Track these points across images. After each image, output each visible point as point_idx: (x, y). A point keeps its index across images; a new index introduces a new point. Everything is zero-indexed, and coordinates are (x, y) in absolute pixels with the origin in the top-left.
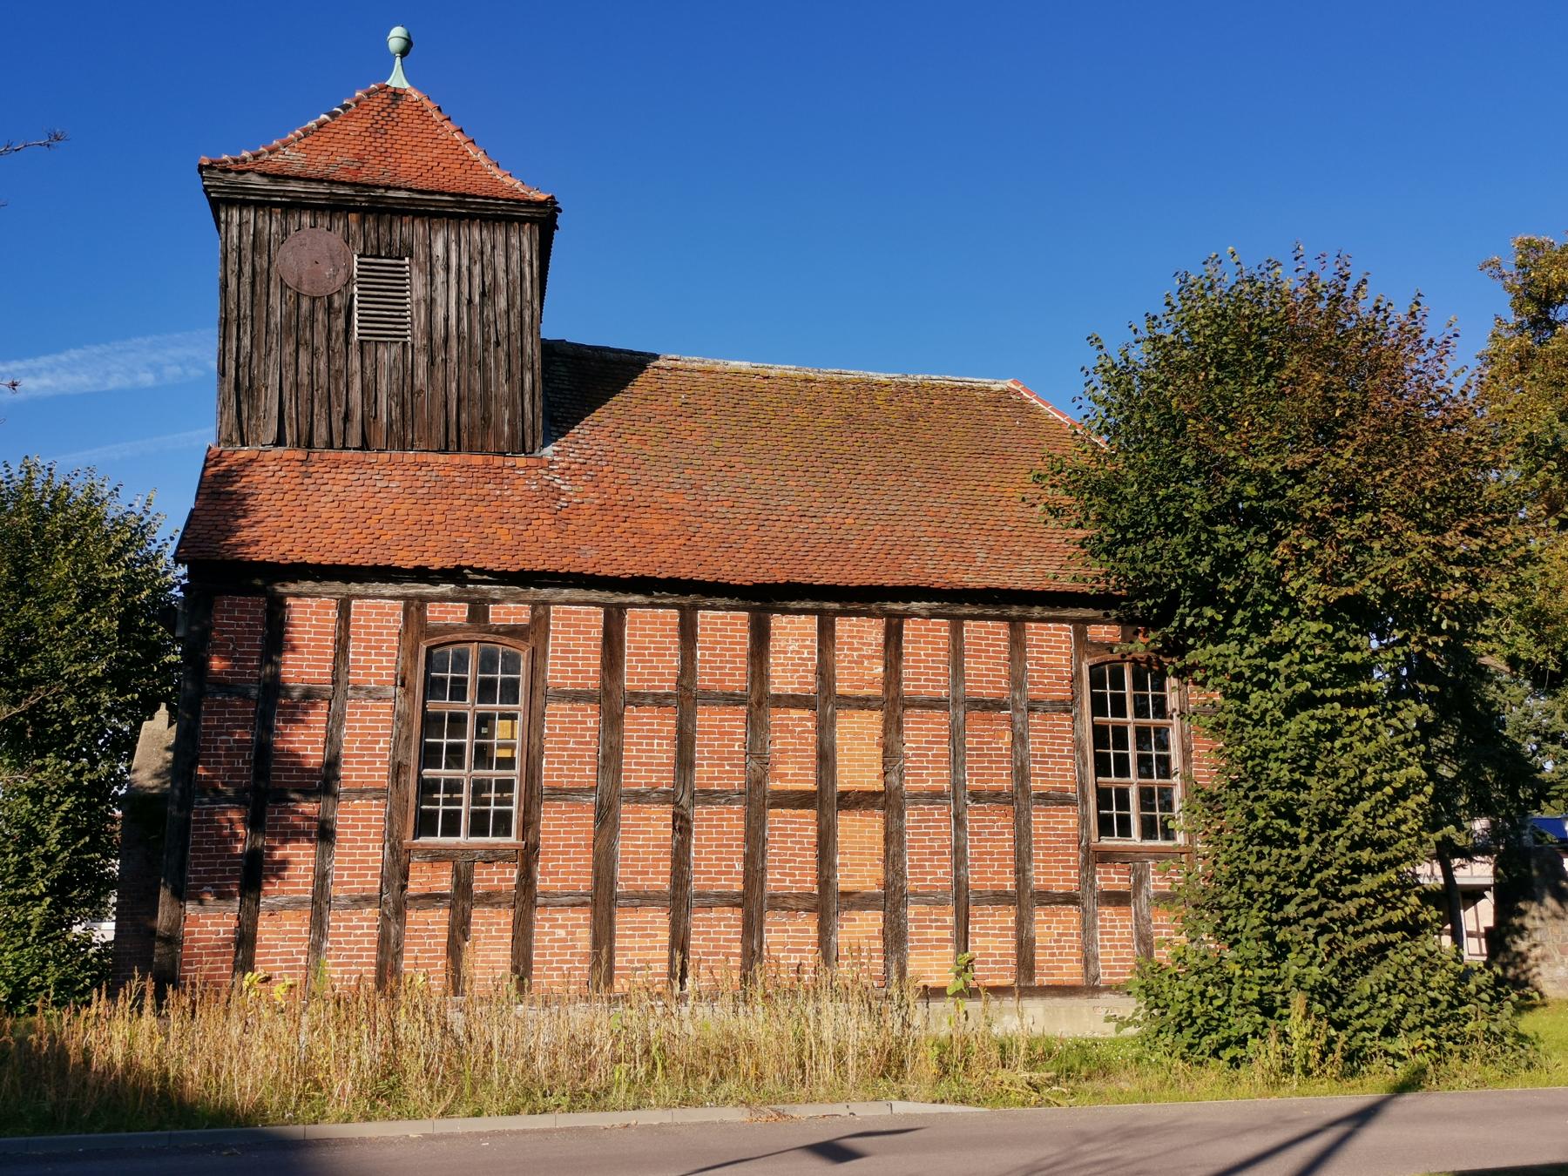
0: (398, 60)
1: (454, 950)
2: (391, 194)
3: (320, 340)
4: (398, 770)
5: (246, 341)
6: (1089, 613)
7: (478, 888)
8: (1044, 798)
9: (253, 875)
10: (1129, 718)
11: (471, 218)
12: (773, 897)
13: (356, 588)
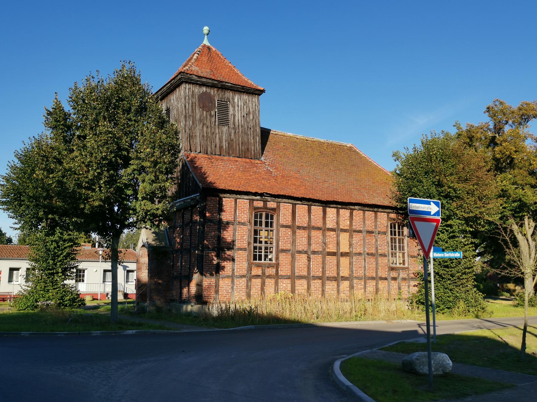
0: (206, 36)
1: (262, 289)
2: (227, 84)
3: (208, 124)
4: (249, 243)
5: (191, 123)
6: (390, 211)
7: (267, 274)
8: (381, 255)
9: (218, 269)
10: (397, 236)
11: (244, 92)
12: (328, 277)
13: (239, 196)
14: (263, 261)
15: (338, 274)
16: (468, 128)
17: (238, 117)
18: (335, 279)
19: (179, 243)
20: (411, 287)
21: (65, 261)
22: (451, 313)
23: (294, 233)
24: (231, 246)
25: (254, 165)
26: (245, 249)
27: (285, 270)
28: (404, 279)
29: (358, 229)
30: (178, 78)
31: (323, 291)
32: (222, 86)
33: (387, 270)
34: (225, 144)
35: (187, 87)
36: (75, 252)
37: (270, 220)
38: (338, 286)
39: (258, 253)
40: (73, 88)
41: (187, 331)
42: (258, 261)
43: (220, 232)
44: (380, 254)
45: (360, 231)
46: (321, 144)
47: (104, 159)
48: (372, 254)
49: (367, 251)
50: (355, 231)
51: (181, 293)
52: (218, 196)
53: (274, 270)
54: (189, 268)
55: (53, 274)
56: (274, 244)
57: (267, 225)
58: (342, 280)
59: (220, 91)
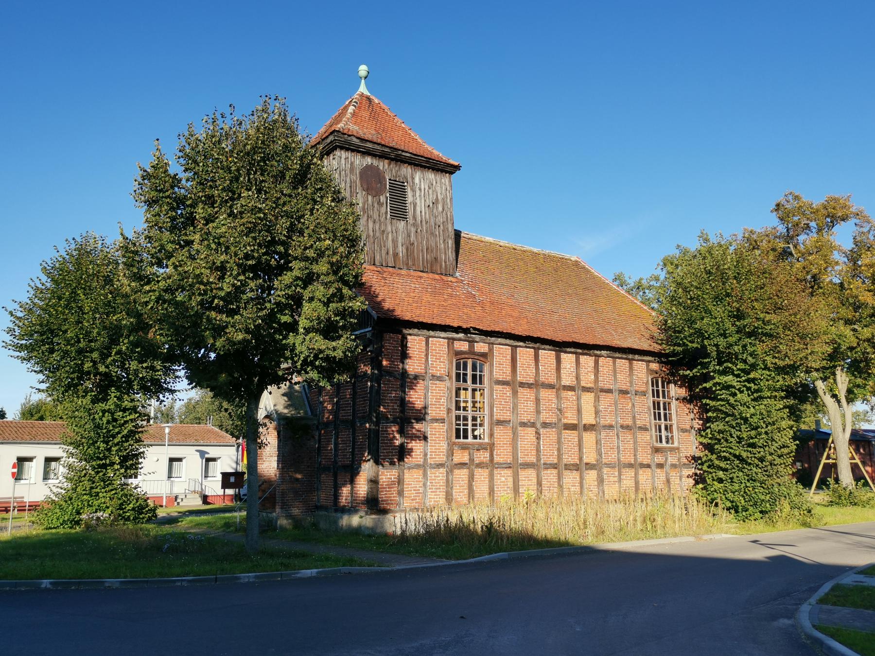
0: (363, 81)
2: (404, 154)
3: (376, 216)
4: (449, 411)
7: (477, 461)
9: (402, 453)
11: (429, 168)
12: (566, 465)
13: (432, 333)
14: (470, 439)
15: (581, 459)
16: (746, 235)
17: (421, 207)
18: (576, 467)
19: (330, 412)
20: (683, 479)
21: (126, 444)
22: (772, 522)
23: (515, 393)
24: (421, 416)
25: (447, 285)
26: (442, 421)
27: (502, 455)
28: (674, 466)
29: (606, 387)
30: (329, 140)
31: (561, 486)
32: (396, 157)
33: (649, 451)
34: (401, 251)
35: (344, 156)
36: (140, 429)
37: (478, 373)
38: (582, 478)
39: (462, 427)
40: (187, 134)
41: (408, 567)
42: (462, 440)
43: (404, 392)
44: (640, 427)
45: (609, 391)
46: (535, 255)
47: (247, 257)
48: (627, 427)
49: (620, 421)
50: (602, 391)
51: (336, 496)
52: (400, 332)
53: (487, 455)
54: (353, 453)
55: (104, 466)
56: (486, 412)
57: (474, 381)
58: (586, 469)
59: (393, 165)
